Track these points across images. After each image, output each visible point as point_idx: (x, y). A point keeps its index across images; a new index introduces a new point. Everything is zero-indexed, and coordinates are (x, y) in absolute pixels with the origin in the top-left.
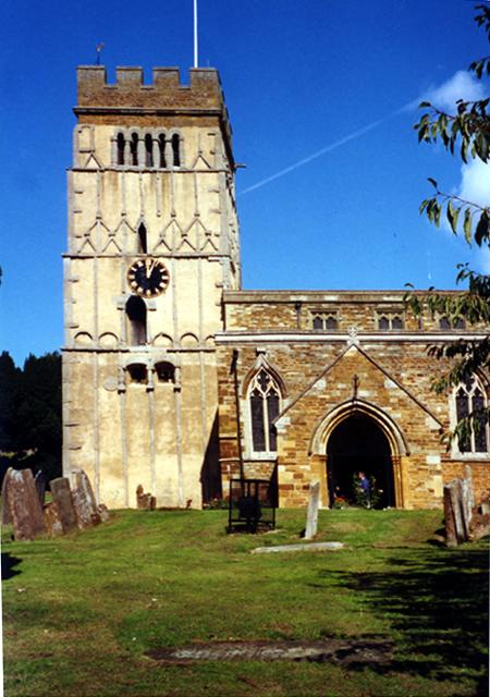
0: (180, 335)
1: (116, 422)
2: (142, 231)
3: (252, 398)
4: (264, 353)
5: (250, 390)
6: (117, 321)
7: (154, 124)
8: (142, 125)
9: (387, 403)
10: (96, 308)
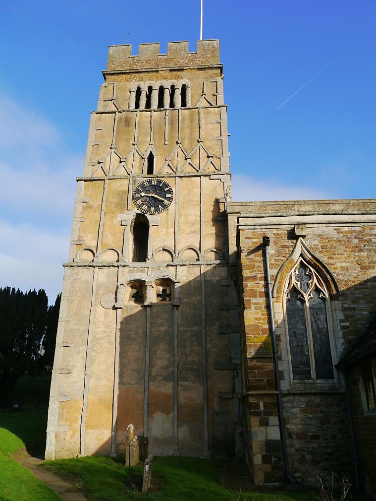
4: (304, 237)
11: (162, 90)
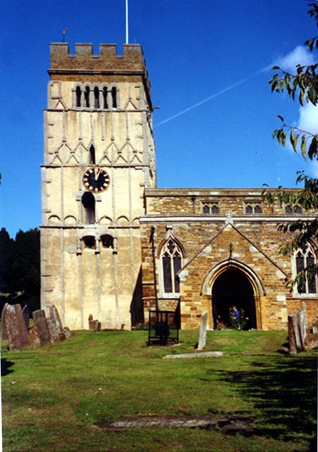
0: (117, 217)
1: (75, 273)
2: (92, 150)
3: (163, 258)
4: (171, 229)
6: (76, 208)
7: (100, 80)
8: (92, 81)
9: (251, 261)
10: (62, 200)
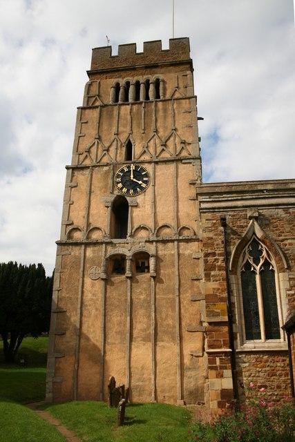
1: (97, 309)
2: (129, 147)
3: (242, 272)
5: (241, 263)
7: (143, 74)
11: (137, 85)
